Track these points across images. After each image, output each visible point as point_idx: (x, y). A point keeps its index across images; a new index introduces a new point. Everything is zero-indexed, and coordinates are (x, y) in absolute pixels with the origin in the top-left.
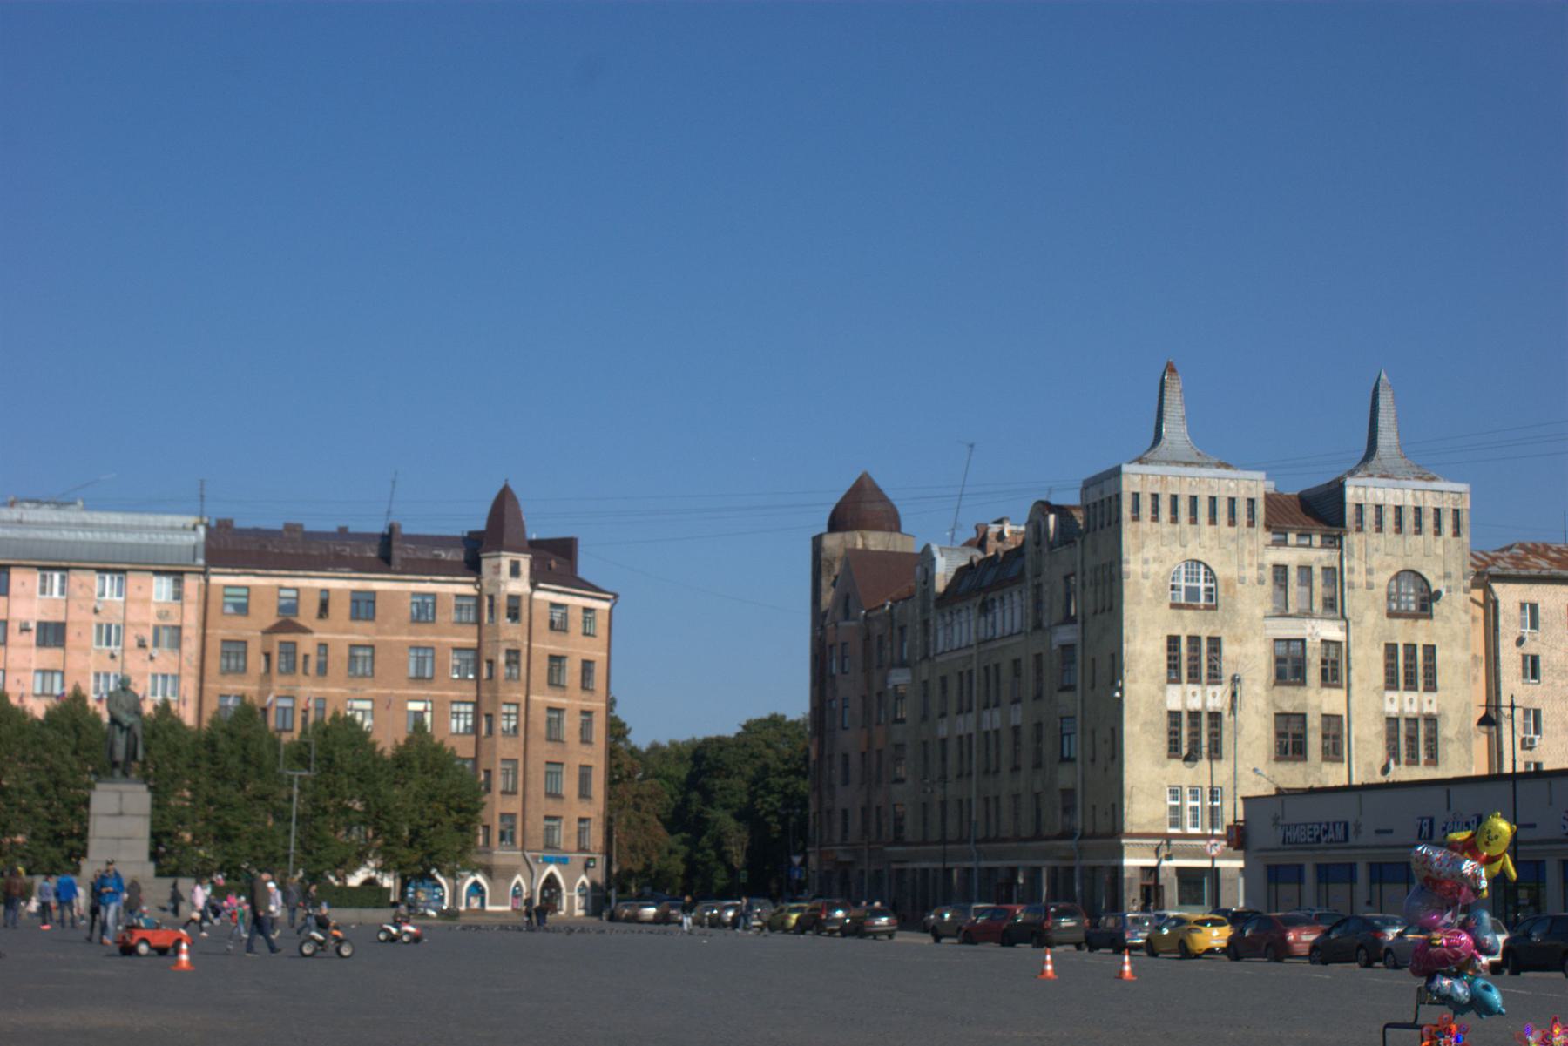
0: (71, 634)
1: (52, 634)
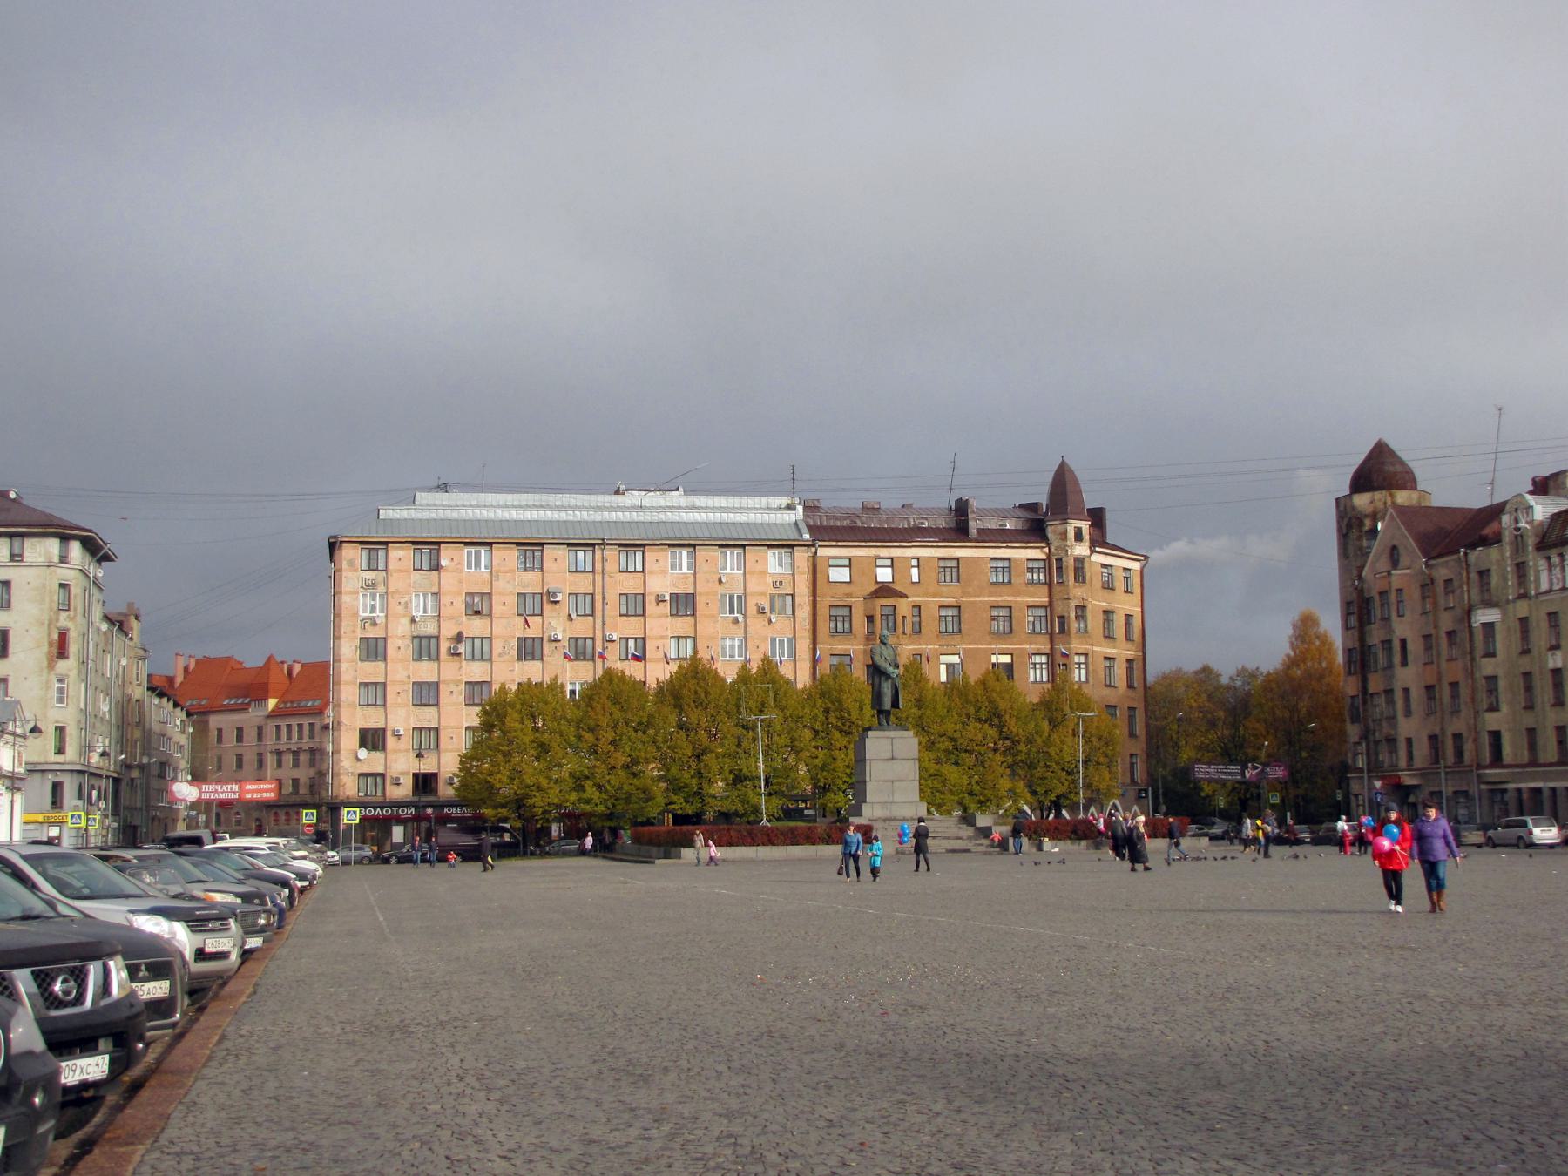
0: (701, 602)
1: (684, 604)
